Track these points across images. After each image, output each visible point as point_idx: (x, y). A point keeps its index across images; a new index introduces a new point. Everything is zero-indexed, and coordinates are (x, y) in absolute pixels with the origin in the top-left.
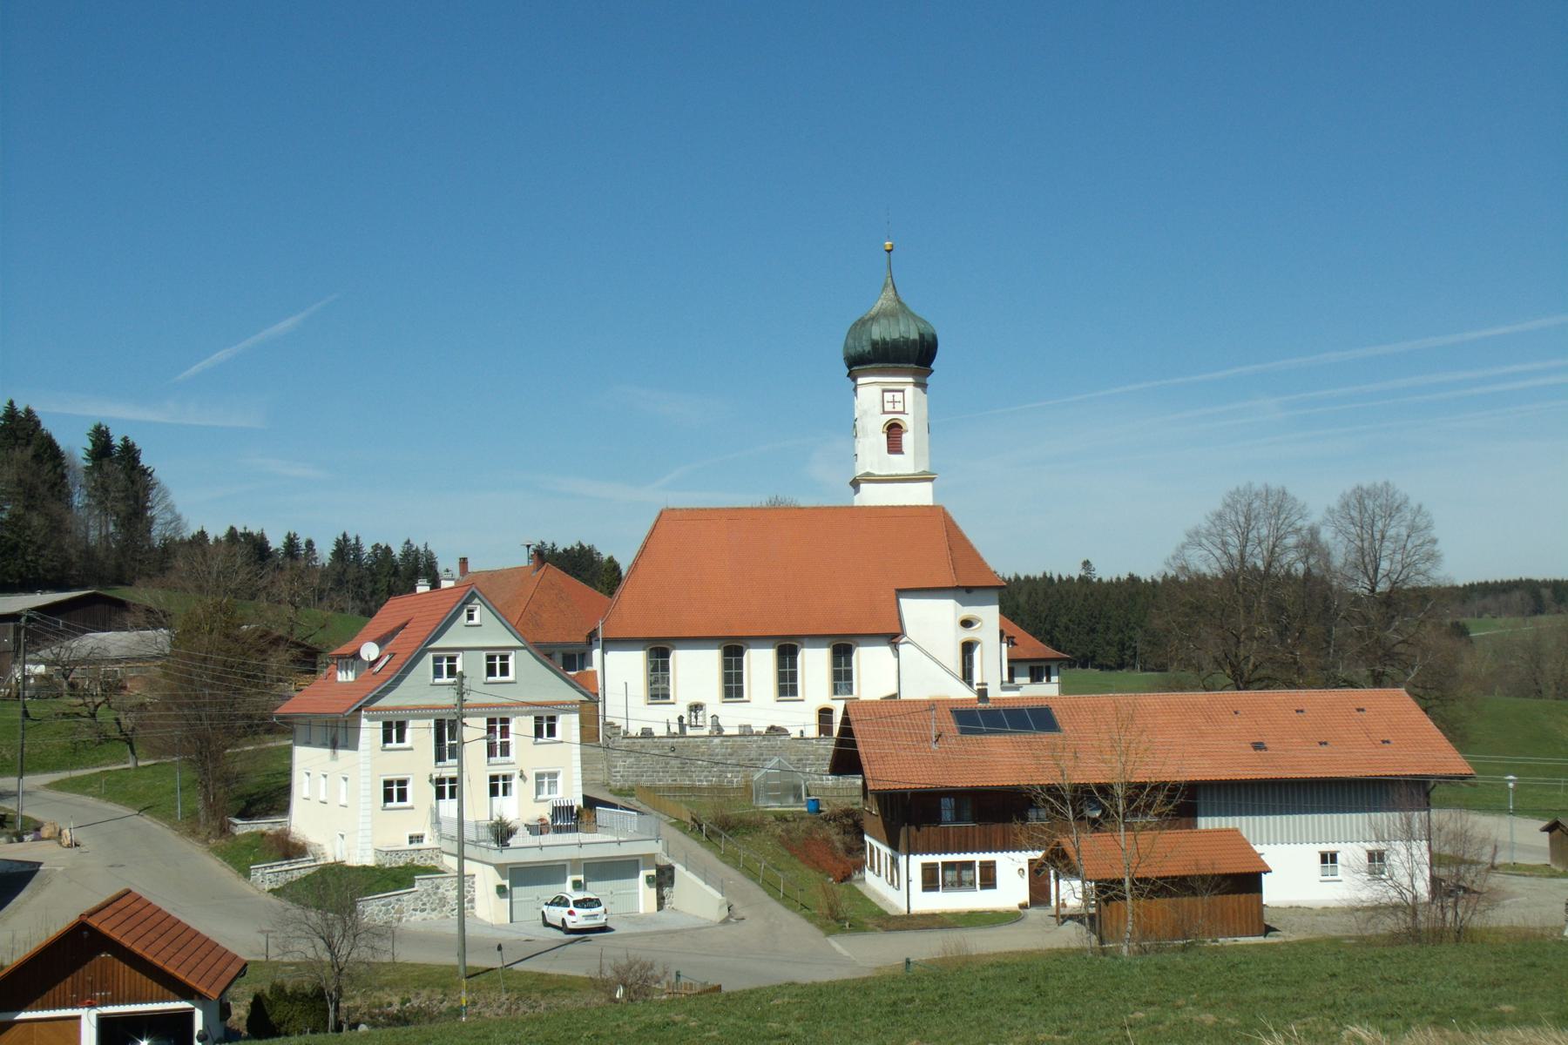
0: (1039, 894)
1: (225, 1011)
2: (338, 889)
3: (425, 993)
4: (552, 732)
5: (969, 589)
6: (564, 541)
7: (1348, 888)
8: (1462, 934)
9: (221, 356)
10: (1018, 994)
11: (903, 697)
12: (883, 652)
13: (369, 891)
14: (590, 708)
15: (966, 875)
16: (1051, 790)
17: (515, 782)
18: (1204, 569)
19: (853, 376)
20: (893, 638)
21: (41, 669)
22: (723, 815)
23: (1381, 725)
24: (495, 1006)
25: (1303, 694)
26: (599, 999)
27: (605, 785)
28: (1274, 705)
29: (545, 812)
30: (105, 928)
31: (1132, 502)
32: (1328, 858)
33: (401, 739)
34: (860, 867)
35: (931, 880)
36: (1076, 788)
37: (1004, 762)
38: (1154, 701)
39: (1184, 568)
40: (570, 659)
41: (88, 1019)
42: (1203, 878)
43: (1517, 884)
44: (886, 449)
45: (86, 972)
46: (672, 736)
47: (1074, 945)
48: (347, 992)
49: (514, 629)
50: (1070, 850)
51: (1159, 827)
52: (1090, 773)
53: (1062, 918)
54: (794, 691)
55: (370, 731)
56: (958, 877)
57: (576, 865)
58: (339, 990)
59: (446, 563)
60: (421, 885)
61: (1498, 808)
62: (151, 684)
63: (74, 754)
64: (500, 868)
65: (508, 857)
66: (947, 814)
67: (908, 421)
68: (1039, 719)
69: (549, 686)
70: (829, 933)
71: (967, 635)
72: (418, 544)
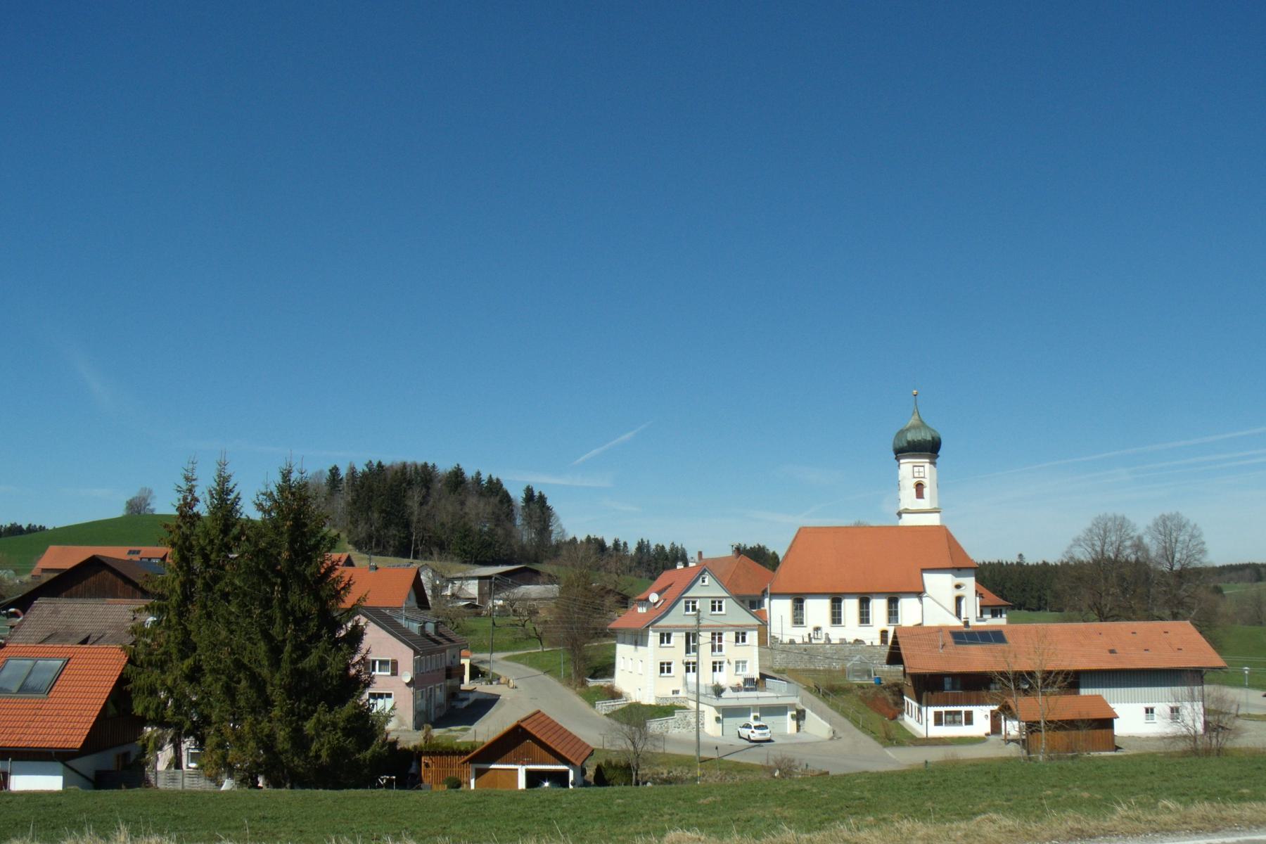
0: (996, 728)
1: (583, 772)
2: (637, 716)
3: (679, 769)
4: (744, 640)
5: (959, 569)
6: (750, 543)
7: (1160, 727)
8: (1220, 752)
9: (595, 451)
10: (984, 780)
11: (925, 624)
12: (914, 601)
13: (653, 717)
14: (763, 628)
15: (957, 718)
16: (1003, 674)
17: (725, 665)
18: (1082, 558)
19: (898, 459)
20: (919, 594)
21: (501, 602)
22: (831, 684)
23: (1178, 641)
24: (714, 777)
25: (1135, 624)
26: (766, 776)
27: (771, 668)
28: (1122, 628)
29: (740, 681)
30: (529, 728)
31: (1044, 527)
32: (1149, 711)
33: (668, 642)
34: (902, 712)
35: (938, 720)
36: (1016, 673)
37: (977, 659)
38: (1056, 627)
39: (1072, 558)
40: (753, 603)
41: (522, 771)
42: (1083, 721)
43: (1250, 725)
44: (915, 496)
45: (520, 749)
46: (804, 643)
47: (1014, 755)
48: (642, 766)
49: (726, 588)
50: (1012, 706)
51: (1060, 694)
52: (1023, 665)
53: (1008, 741)
54: (868, 621)
55: (653, 637)
56: (953, 718)
57: (755, 708)
58: (638, 765)
59: (692, 554)
60: (678, 715)
61: (1239, 684)
62: (550, 611)
63: (515, 644)
64: (717, 708)
65: (721, 703)
66: (947, 686)
67: (926, 482)
68: (996, 637)
69: (742, 617)
70: (885, 746)
71: (958, 593)
72: (678, 544)
